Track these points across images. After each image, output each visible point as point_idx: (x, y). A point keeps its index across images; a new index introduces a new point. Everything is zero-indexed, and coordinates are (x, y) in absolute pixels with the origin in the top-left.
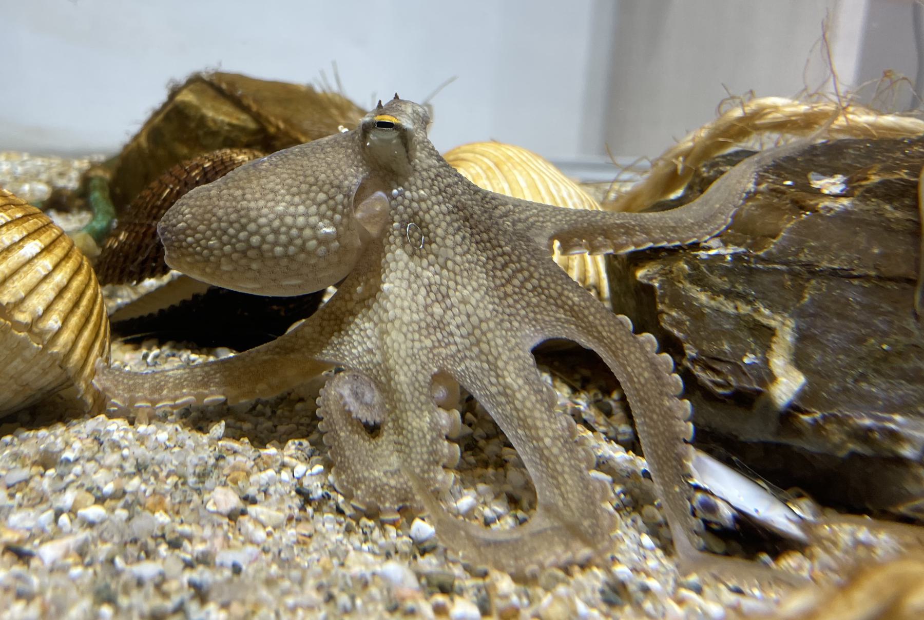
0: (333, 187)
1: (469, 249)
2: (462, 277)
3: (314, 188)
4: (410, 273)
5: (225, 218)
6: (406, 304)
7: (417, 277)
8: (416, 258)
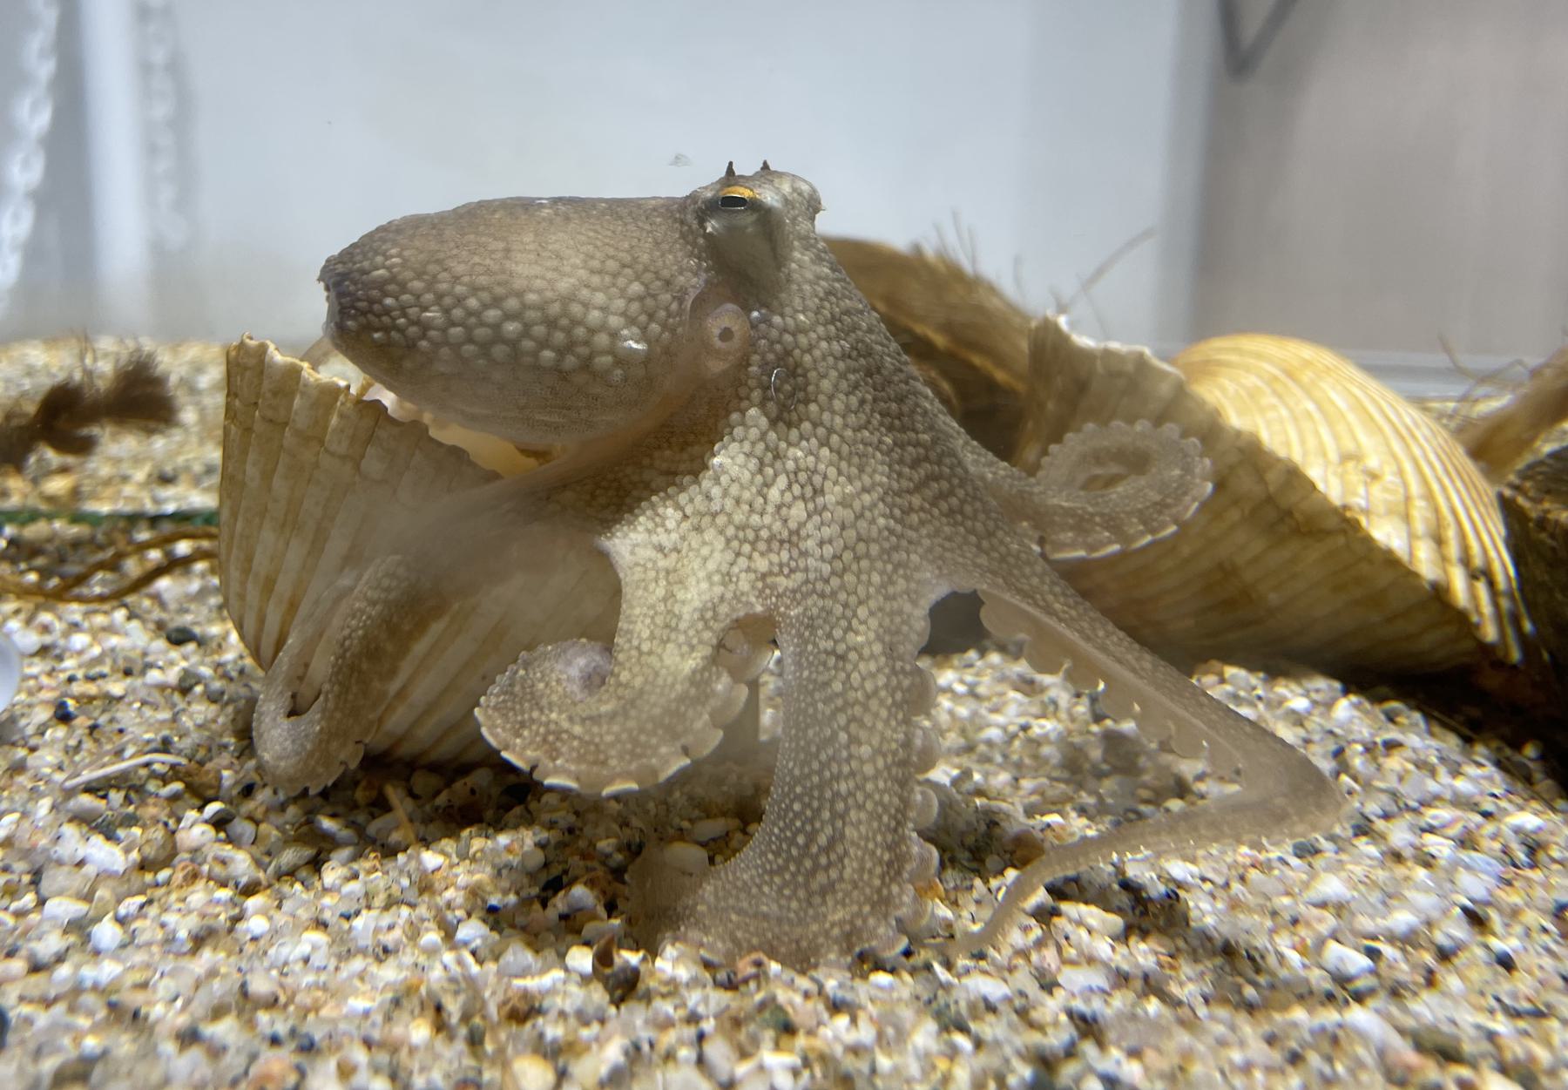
0: (658, 279)
1: (869, 422)
2: (850, 465)
3: (628, 271)
4: (767, 448)
5: (466, 279)
6: (746, 495)
7: (777, 457)
8: (781, 424)
